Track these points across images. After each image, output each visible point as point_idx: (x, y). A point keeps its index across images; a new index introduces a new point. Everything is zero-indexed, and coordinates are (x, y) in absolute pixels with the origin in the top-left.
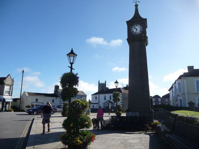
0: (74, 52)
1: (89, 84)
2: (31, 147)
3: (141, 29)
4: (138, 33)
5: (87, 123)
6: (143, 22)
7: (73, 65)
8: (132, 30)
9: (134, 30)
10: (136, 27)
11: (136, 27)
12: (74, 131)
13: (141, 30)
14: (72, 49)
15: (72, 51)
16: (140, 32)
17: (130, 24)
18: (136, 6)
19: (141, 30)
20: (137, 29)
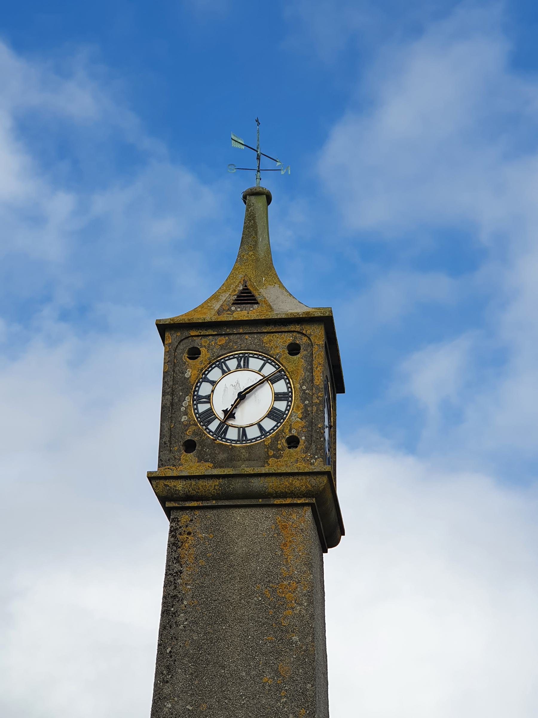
4: (253, 433)
13: (281, 406)
19: (281, 406)
20: (245, 396)
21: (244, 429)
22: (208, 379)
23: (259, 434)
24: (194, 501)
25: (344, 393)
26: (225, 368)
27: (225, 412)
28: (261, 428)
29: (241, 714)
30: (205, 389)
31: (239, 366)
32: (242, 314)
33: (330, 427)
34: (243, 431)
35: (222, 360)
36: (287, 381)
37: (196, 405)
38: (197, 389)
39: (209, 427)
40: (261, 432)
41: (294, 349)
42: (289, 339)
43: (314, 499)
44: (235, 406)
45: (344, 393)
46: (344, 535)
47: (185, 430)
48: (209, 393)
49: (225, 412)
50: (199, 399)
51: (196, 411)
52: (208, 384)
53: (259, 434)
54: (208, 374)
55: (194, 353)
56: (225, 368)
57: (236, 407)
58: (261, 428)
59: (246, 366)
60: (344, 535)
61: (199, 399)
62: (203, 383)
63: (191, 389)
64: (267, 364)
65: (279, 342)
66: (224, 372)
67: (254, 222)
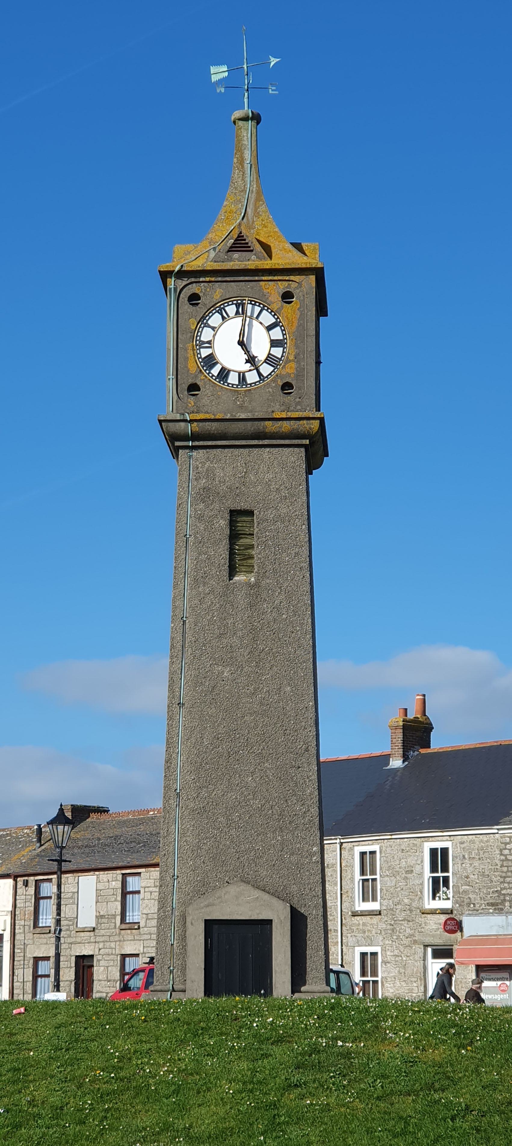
3: (274, 343)
21: (244, 373)
22: (208, 324)
23: (258, 379)
24: (201, 440)
26: (240, 310)
29: (162, 1144)
30: (206, 335)
32: (238, 261)
34: (270, 359)
35: (222, 306)
36: (257, 304)
38: (199, 334)
39: (212, 371)
40: (260, 378)
41: (287, 297)
42: (282, 287)
43: (308, 441)
44: (247, 351)
46: (328, 456)
48: (210, 338)
50: (201, 344)
51: (199, 356)
52: (210, 329)
53: (258, 379)
54: (209, 319)
55: (194, 298)
57: (248, 352)
60: (328, 456)
61: (201, 344)
62: (205, 328)
63: (194, 335)
65: (274, 289)
66: (223, 318)
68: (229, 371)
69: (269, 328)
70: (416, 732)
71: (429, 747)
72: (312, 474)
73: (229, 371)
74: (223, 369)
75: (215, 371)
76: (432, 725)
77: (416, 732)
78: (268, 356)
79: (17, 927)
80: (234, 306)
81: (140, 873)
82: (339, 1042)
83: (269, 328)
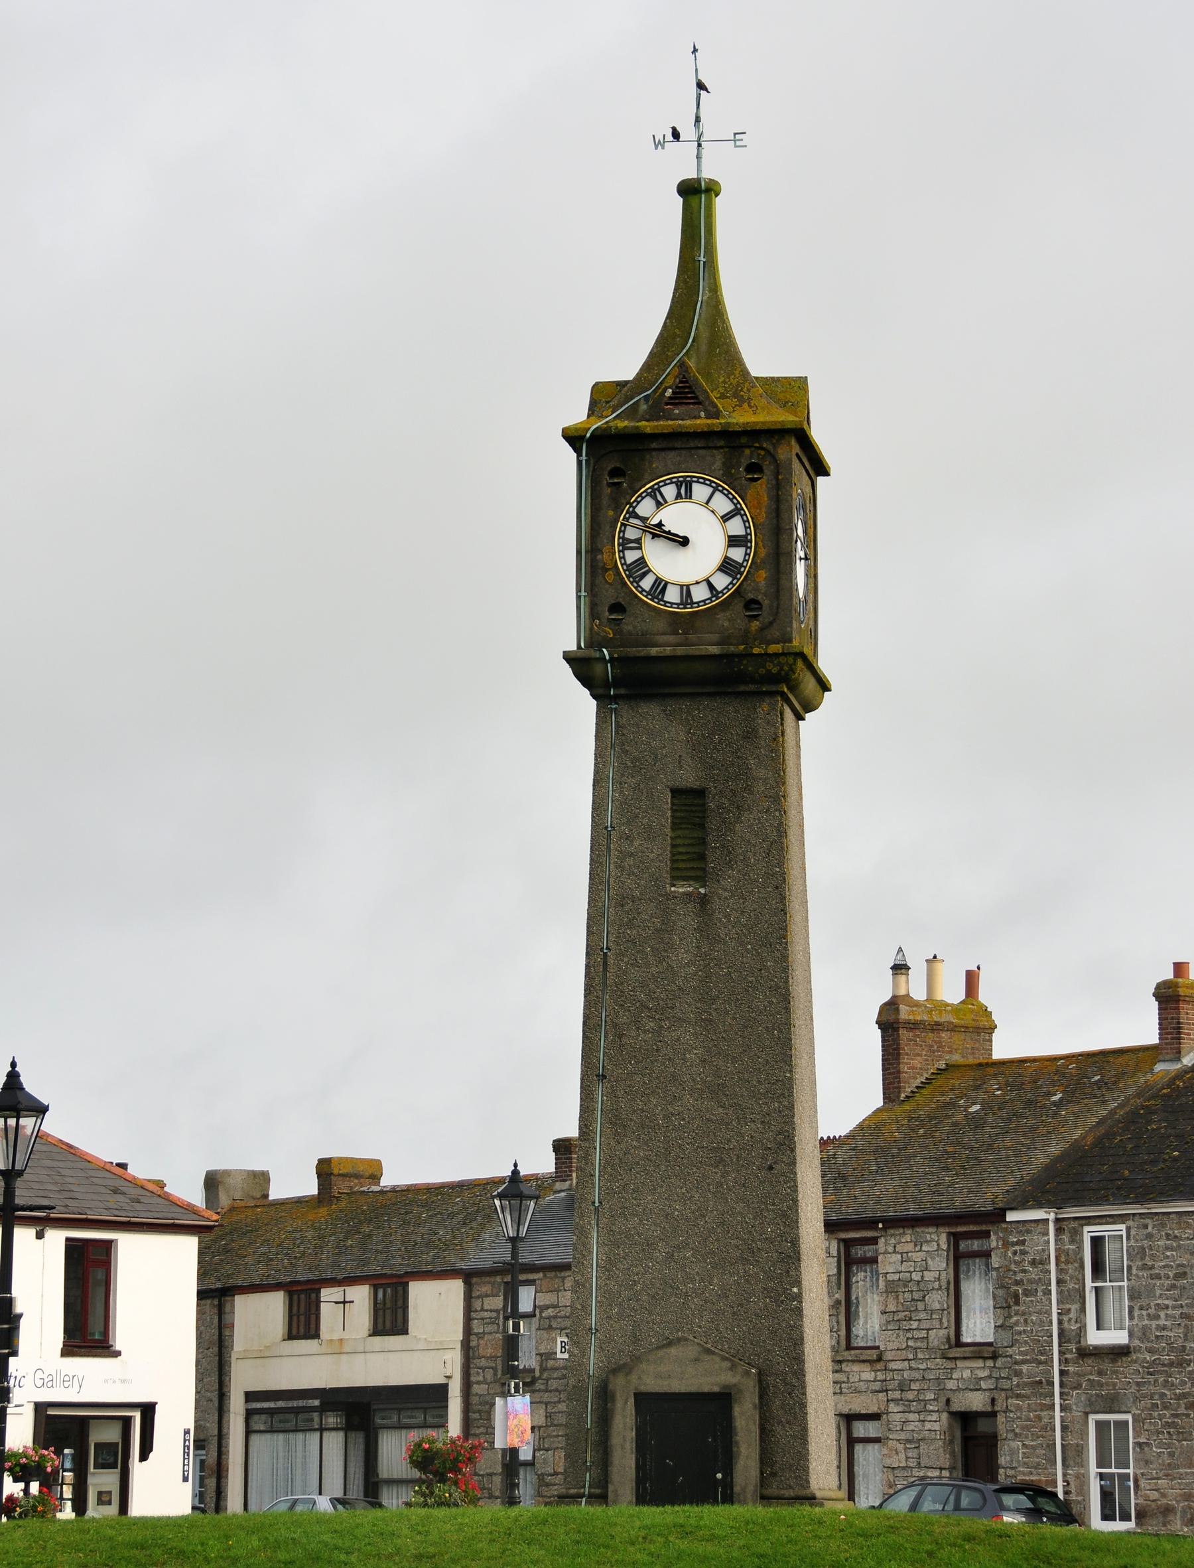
0: (32, 1085)
1: (161, 1184)
2: (813, 1447)
3: (733, 541)
4: (700, 593)
5: (795, 1290)
6: (766, 455)
7: (19, 1183)
8: (654, 493)
9: (664, 563)
10: (675, 516)
11: (675, 516)
12: (998, 1089)
13: (737, 554)
14: (13, 1065)
15: (13, 1076)
16: (721, 581)
17: (620, 453)
18: (696, 193)
19: (737, 554)
20: (692, 542)
21: (688, 586)
23: (709, 595)
25: (804, 380)
26: (660, 498)
27: (660, 525)
28: (711, 587)
31: (679, 496)
33: (806, 546)
37: (623, 551)
39: (641, 584)
45: (804, 380)
47: (607, 586)
49: (660, 525)
53: (709, 595)
56: (660, 498)
58: (711, 587)
59: (689, 495)
64: (718, 494)
67: (762, 1473)
68: (726, 557)
69: (726, 518)
70: (40, 1236)
71: (68, 1239)
72: (803, 719)
73: (666, 583)
74: (658, 581)
75: (647, 583)
76: (988, 1014)
77: (40, 1236)
78: (724, 561)
79: (473, 1371)
80: (674, 486)
81: (534, 1281)
82: (8, 1480)
83: (726, 518)
